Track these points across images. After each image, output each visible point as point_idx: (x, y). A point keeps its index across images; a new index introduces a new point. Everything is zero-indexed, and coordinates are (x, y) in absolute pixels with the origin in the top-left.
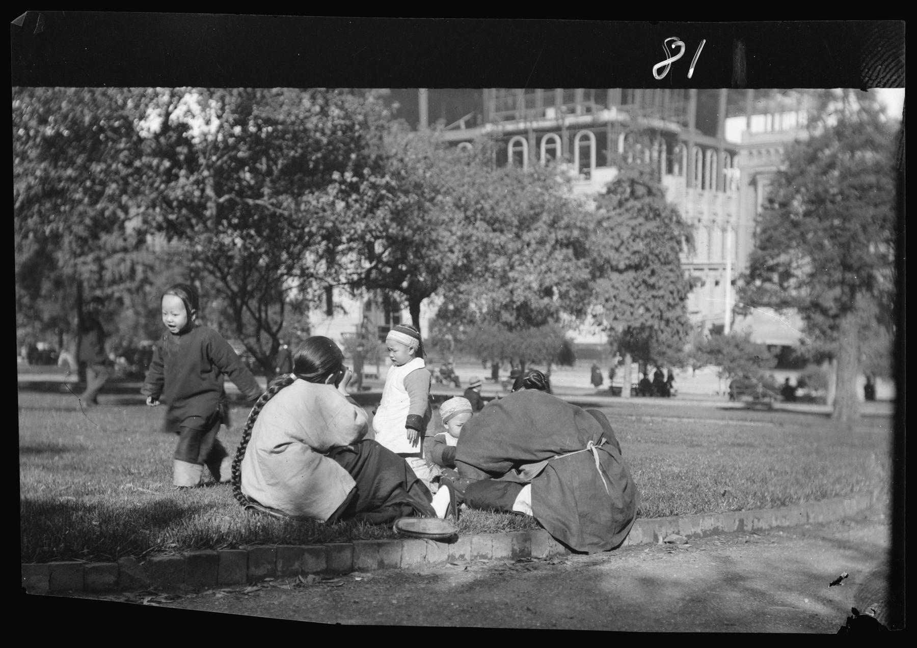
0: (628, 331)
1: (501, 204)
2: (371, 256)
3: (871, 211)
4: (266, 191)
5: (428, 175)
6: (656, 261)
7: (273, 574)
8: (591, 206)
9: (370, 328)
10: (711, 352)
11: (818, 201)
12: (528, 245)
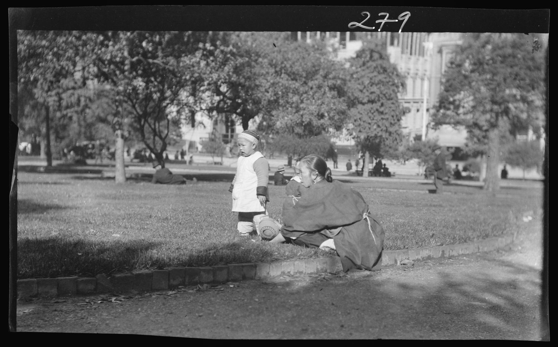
0: (367, 139)
1: (296, 64)
2: (219, 93)
3: (509, 70)
4: (160, 54)
5: (254, 46)
6: (384, 98)
7: (183, 284)
8: (347, 65)
9: (217, 135)
10: (414, 151)
11: (479, 64)
12: (312, 88)
